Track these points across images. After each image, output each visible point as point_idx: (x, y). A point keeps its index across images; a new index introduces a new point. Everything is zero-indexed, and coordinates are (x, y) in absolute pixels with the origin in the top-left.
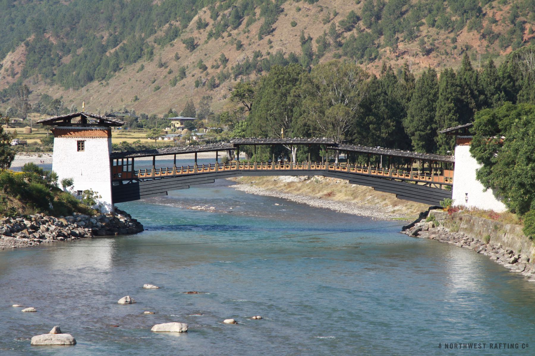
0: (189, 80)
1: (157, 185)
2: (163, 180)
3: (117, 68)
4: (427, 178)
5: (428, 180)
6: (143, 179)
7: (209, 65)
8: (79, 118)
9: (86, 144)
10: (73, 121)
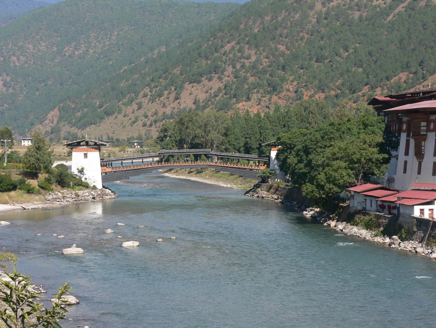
0: (140, 123)
1: (124, 174)
2: (127, 172)
3: (102, 118)
4: (257, 167)
5: (257, 168)
6: (117, 171)
7: (149, 115)
8: (84, 142)
9: (88, 154)
10: (81, 144)
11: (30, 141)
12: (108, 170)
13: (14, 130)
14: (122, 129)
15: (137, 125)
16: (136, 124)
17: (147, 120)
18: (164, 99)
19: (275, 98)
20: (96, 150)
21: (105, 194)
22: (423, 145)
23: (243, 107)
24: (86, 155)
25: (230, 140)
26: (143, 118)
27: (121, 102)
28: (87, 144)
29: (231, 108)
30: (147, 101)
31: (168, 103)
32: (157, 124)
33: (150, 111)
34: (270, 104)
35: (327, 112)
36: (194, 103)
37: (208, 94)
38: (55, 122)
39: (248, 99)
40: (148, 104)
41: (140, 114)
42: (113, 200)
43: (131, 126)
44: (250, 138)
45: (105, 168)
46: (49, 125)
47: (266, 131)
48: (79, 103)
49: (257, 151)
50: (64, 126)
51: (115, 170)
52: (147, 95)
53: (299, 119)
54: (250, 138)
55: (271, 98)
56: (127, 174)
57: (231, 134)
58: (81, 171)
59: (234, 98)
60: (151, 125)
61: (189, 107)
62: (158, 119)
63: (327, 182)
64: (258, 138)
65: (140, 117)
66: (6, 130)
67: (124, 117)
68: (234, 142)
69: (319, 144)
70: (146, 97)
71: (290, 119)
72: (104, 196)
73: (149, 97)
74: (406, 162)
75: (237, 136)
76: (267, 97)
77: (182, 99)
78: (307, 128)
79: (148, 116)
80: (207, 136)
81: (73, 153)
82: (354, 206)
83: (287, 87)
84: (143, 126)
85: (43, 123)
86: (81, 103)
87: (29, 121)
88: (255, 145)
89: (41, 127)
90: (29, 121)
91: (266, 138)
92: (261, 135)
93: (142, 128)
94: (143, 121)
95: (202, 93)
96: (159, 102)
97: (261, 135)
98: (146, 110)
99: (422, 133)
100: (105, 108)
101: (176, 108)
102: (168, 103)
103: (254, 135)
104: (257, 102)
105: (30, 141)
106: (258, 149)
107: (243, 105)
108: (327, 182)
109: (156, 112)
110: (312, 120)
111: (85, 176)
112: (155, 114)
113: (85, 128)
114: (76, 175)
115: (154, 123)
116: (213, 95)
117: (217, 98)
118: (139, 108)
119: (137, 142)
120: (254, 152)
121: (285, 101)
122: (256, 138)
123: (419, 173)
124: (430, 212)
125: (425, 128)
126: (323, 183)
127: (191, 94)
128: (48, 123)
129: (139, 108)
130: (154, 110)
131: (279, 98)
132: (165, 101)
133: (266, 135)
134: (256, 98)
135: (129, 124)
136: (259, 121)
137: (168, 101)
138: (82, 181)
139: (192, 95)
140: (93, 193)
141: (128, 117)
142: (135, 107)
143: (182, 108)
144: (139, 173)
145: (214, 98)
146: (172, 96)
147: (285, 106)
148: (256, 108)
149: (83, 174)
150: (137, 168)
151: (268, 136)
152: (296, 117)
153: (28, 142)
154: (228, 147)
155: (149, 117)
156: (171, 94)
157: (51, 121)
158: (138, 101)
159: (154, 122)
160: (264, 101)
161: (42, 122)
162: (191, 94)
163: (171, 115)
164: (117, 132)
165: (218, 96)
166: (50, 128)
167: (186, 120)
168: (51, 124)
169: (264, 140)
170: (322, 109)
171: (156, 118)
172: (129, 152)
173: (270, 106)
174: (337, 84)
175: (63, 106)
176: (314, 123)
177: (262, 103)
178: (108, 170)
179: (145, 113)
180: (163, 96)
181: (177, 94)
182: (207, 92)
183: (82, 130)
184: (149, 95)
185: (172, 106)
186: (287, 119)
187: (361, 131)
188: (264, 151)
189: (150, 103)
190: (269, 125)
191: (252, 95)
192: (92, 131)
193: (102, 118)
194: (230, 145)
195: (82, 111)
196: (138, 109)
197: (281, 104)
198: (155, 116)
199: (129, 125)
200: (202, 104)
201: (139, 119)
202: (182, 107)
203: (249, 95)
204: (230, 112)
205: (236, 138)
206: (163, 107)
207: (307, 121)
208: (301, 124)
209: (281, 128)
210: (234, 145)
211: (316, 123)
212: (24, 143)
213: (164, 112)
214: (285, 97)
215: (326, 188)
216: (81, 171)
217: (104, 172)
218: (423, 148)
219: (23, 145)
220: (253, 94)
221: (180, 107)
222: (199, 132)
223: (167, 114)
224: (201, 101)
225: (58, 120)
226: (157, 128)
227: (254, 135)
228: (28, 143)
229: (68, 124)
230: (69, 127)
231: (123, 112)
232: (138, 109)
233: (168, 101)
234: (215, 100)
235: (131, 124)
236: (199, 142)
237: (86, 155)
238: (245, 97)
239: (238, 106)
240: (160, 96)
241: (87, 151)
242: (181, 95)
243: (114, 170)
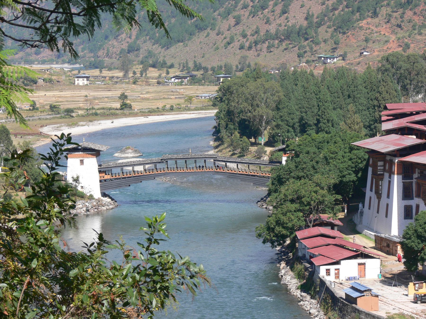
0: (236, 44)
3: (191, 34)
7: (249, 33)
11: (85, 79)
12: (107, 177)
13: (83, 44)
14: (214, 52)
15: (233, 47)
16: (231, 45)
17: (245, 40)
18: (268, 12)
19: (409, 14)
20: (93, 156)
21: (101, 204)
22: (380, 184)
23: (367, 26)
25: (282, 114)
26: (241, 38)
27: (217, 12)
29: (352, 27)
30: (247, 14)
31: (273, 17)
32: (259, 46)
33: (250, 28)
34: (402, 22)
35: (420, 67)
36: (306, 19)
37: (324, 6)
38: (133, 37)
39: (375, 14)
40: (248, 18)
41: (238, 32)
42: (111, 211)
43: (225, 49)
44: (306, 113)
45: (104, 174)
46: (126, 41)
47: (326, 104)
48: (165, 10)
49: (314, 127)
50: (145, 42)
52: (248, 6)
53: (369, 87)
54: (306, 113)
55: (404, 13)
57: (283, 108)
58: (76, 180)
59: (357, 12)
60: (250, 48)
61: (299, 24)
62: (259, 39)
63: (276, 225)
64: (316, 113)
65: (238, 36)
66: (3, 129)
67: (218, 35)
68: (287, 118)
69: (292, 174)
70: (246, 8)
71: (356, 88)
72: (100, 207)
73: (250, 8)
74: (370, 198)
75: (291, 110)
76: (399, 13)
77: (290, 12)
78: (376, 99)
79: (247, 35)
80: (255, 110)
84: (240, 49)
85: (119, 38)
86: (167, 12)
87: (103, 31)
88: (312, 121)
89: (115, 43)
90: (103, 31)
91: (325, 113)
92: (319, 109)
93: (238, 51)
94: (241, 41)
95: (317, 5)
96: (262, 16)
97: (319, 109)
98: (245, 27)
99: (379, 173)
100: (196, 20)
101: (283, 24)
102: (273, 17)
103: (311, 108)
104: (385, 19)
105: (85, 79)
106: (316, 125)
107: (368, 23)
108: (276, 225)
109: (257, 30)
110: (383, 89)
111: (80, 185)
112: (256, 32)
113: (171, 47)
114: (71, 184)
115: (254, 44)
116: (330, 8)
117: (336, 12)
118: (237, 23)
119: (223, 77)
120: (311, 129)
121: (422, 18)
122: (313, 112)
123: (378, 212)
124: (336, 272)
125: (382, 168)
126: (272, 226)
127: (302, 6)
128: (124, 37)
129: (237, 23)
130: (255, 27)
131: (415, 13)
132: (269, 16)
133: (324, 109)
134: (385, 12)
135: (222, 45)
136: (318, 92)
137: (273, 15)
138: (77, 190)
139: (304, 8)
140: (87, 204)
141: (222, 35)
142: (232, 21)
143: (290, 25)
145: (332, 12)
146: (279, 9)
147: (421, 24)
148: (384, 27)
149: (79, 183)
151: (328, 110)
152: (364, 85)
153: (83, 80)
154: (280, 123)
155: (248, 37)
156: (278, 6)
157: (129, 35)
158: (236, 14)
159: (254, 43)
160: (396, 18)
161: (117, 36)
162: (302, 6)
163: (276, 35)
164: (207, 56)
165: (337, 9)
166: (127, 45)
167: (234, 88)
168: (128, 40)
169: (322, 115)
170: (414, 63)
171: (257, 38)
172: (203, 98)
173: (403, 24)
175: (144, 14)
176: (384, 93)
177: (393, 21)
178: (107, 177)
179: (244, 31)
181: (284, 5)
183: (165, 50)
184: (250, 6)
185: (278, 22)
186: (352, 88)
187: (346, 155)
188: (322, 128)
189: (251, 17)
190: (329, 97)
191: (380, 8)
192: (178, 52)
193: (192, 33)
194: (282, 121)
195: (168, 21)
196: (236, 25)
197: (417, 21)
198: (256, 35)
199: (222, 47)
200: (315, 20)
201: (235, 38)
202: (290, 24)
203: (376, 9)
204: (350, 32)
205: (289, 112)
206: (266, 23)
207: (376, 90)
208: (370, 94)
209: (345, 99)
210: (287, 121)
211: (387, 92)
212: (78, 82)
213: (267, 31)
214: (421, 13)
215: (275, 231)
216: (76, 180)
218: (380, 187)
219: (76, 84)
220: (382, 8)
221: (287, 24)
222: (244, 105)
223: (271, 33)
224: (315, 16)
225: (137, 34)
226: (258, 52)
227: (311, 108)
228: (83, 82)
229: (150, 39)
230: (151, 44)
231: (217, 28)
232: (236, 25)
233: (273, 15)
234: (333, 15)
235: (225, 46)
236: (245, 118)
238: (371, 12)
239: (360, 25)
240: (263, 8)
241: (83, 157)
242: (290, 7)
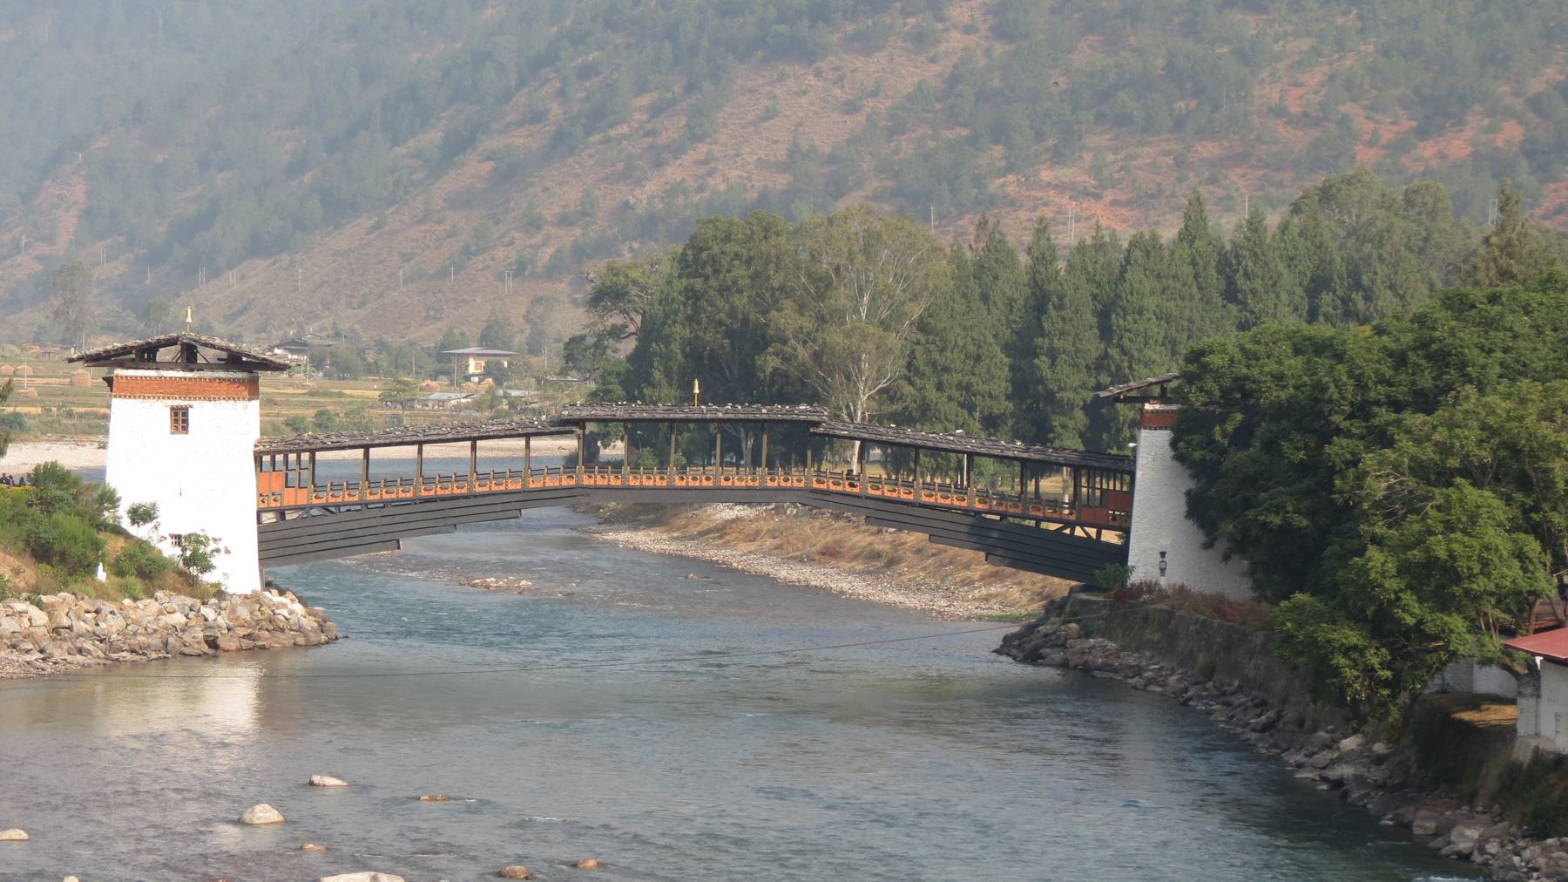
2: (390, 510)
6: (338, 506)
24: (180, 417)
28: (189, 355)
51: (326, 498)
56: (389, 520)
81: (116, 402)
82: (1537, 735)
83: (1275, 96)
144: (454, 521)
150: (440, 493)
174: (1536, 86)
180: (624, 121)
182: (851, 108)
217: (273, 505)
237: (180, 417)
243: (323, 501)
